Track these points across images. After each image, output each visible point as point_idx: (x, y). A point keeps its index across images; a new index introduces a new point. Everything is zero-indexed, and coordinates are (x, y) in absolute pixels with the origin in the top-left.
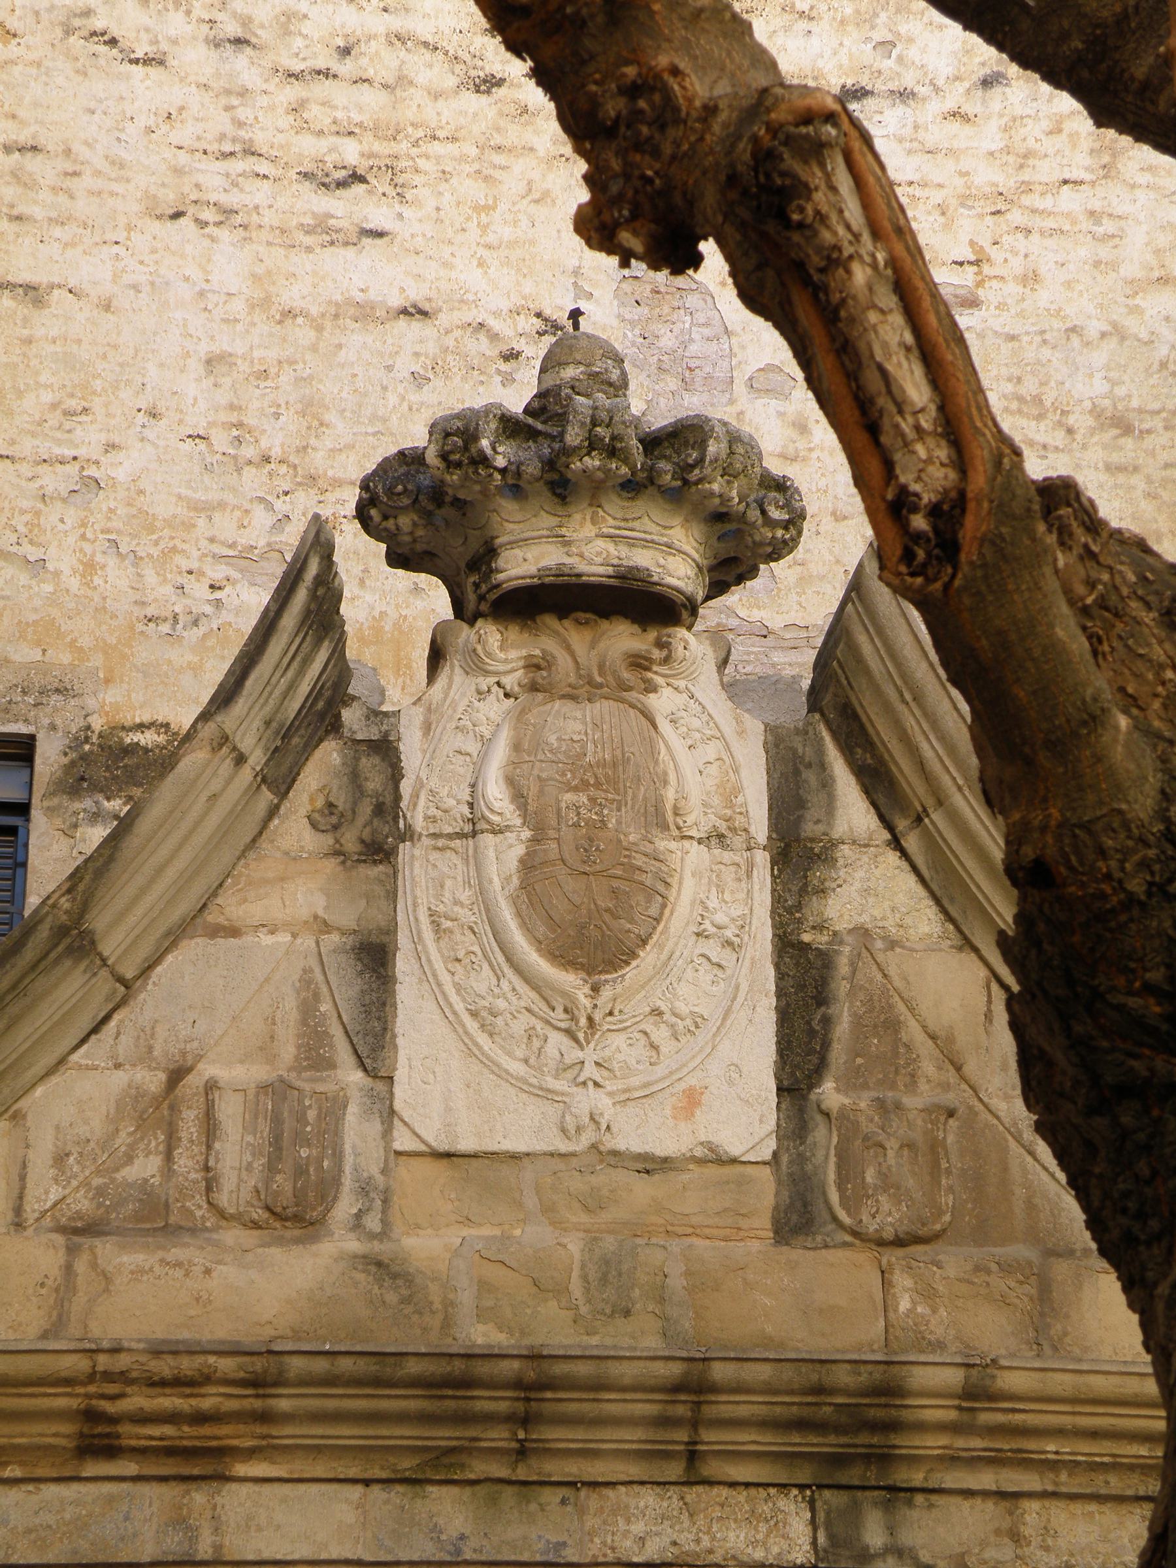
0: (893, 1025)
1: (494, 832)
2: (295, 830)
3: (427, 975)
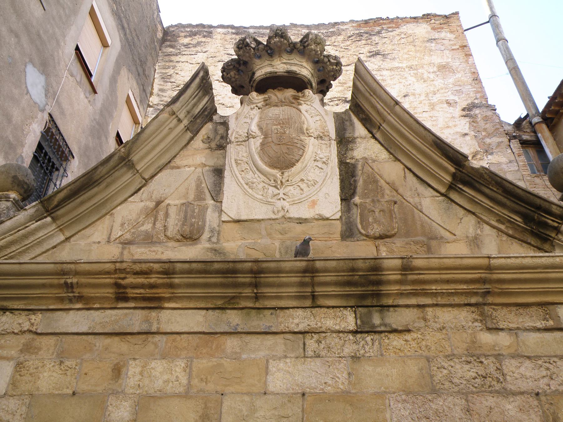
0: (376, 182)
1: (253, 138)
2: (198, 143)
3: (234, 175)
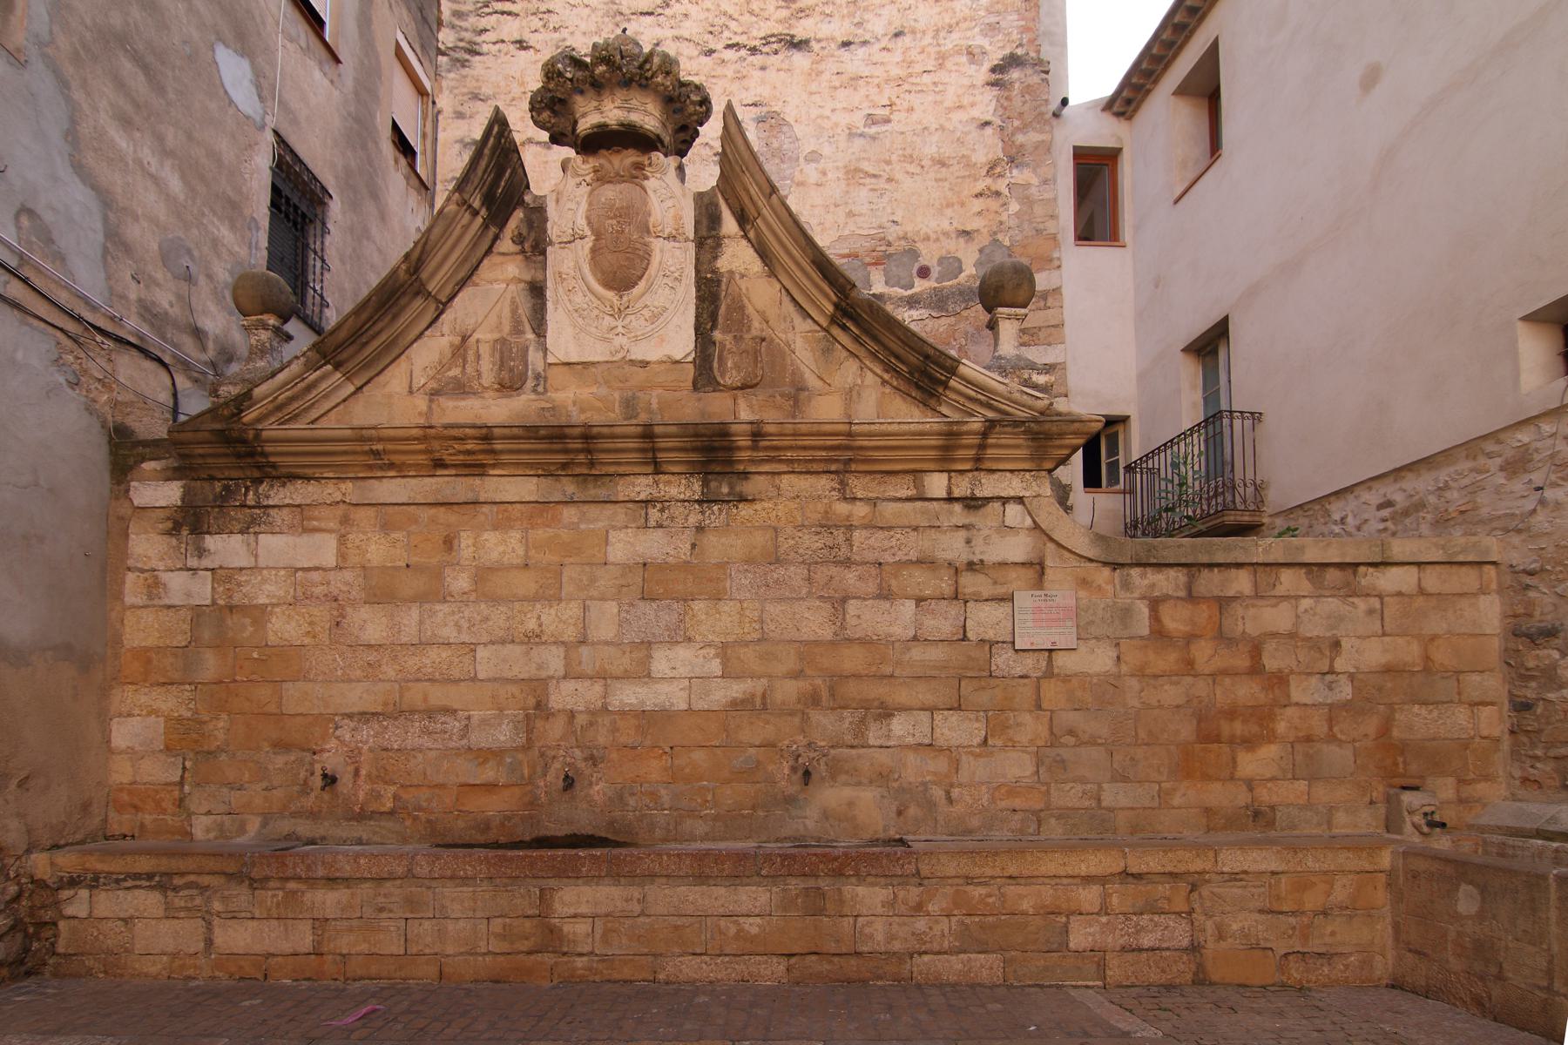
0: (742, 308)
2: (506, 244)
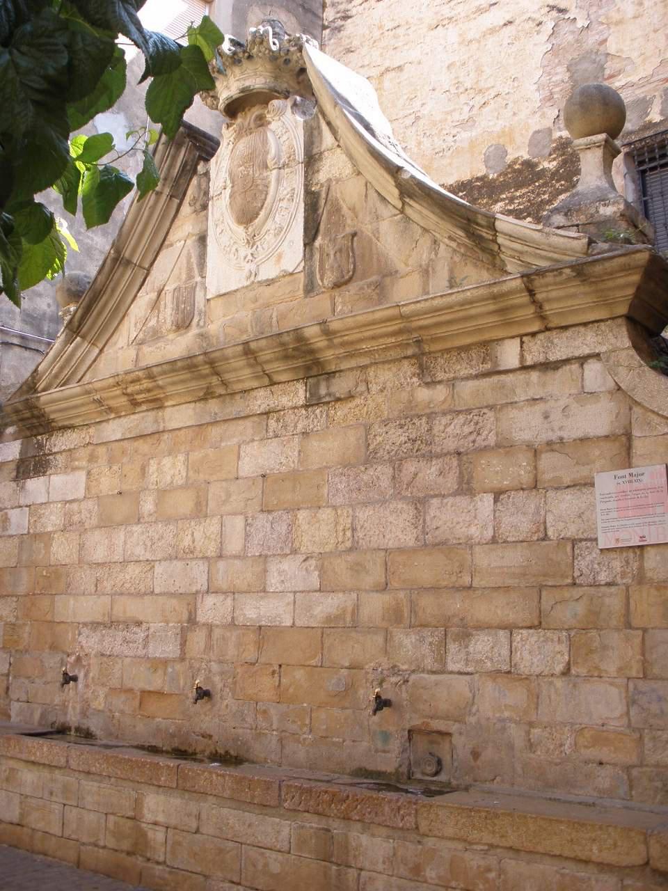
2: (186, 209)
